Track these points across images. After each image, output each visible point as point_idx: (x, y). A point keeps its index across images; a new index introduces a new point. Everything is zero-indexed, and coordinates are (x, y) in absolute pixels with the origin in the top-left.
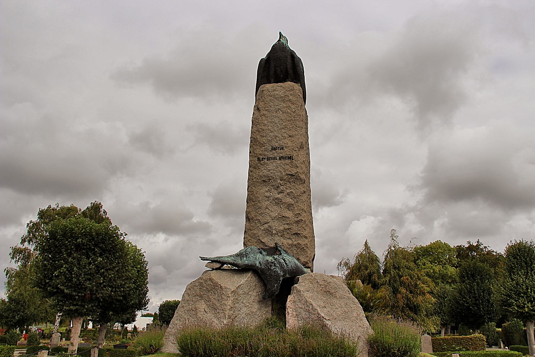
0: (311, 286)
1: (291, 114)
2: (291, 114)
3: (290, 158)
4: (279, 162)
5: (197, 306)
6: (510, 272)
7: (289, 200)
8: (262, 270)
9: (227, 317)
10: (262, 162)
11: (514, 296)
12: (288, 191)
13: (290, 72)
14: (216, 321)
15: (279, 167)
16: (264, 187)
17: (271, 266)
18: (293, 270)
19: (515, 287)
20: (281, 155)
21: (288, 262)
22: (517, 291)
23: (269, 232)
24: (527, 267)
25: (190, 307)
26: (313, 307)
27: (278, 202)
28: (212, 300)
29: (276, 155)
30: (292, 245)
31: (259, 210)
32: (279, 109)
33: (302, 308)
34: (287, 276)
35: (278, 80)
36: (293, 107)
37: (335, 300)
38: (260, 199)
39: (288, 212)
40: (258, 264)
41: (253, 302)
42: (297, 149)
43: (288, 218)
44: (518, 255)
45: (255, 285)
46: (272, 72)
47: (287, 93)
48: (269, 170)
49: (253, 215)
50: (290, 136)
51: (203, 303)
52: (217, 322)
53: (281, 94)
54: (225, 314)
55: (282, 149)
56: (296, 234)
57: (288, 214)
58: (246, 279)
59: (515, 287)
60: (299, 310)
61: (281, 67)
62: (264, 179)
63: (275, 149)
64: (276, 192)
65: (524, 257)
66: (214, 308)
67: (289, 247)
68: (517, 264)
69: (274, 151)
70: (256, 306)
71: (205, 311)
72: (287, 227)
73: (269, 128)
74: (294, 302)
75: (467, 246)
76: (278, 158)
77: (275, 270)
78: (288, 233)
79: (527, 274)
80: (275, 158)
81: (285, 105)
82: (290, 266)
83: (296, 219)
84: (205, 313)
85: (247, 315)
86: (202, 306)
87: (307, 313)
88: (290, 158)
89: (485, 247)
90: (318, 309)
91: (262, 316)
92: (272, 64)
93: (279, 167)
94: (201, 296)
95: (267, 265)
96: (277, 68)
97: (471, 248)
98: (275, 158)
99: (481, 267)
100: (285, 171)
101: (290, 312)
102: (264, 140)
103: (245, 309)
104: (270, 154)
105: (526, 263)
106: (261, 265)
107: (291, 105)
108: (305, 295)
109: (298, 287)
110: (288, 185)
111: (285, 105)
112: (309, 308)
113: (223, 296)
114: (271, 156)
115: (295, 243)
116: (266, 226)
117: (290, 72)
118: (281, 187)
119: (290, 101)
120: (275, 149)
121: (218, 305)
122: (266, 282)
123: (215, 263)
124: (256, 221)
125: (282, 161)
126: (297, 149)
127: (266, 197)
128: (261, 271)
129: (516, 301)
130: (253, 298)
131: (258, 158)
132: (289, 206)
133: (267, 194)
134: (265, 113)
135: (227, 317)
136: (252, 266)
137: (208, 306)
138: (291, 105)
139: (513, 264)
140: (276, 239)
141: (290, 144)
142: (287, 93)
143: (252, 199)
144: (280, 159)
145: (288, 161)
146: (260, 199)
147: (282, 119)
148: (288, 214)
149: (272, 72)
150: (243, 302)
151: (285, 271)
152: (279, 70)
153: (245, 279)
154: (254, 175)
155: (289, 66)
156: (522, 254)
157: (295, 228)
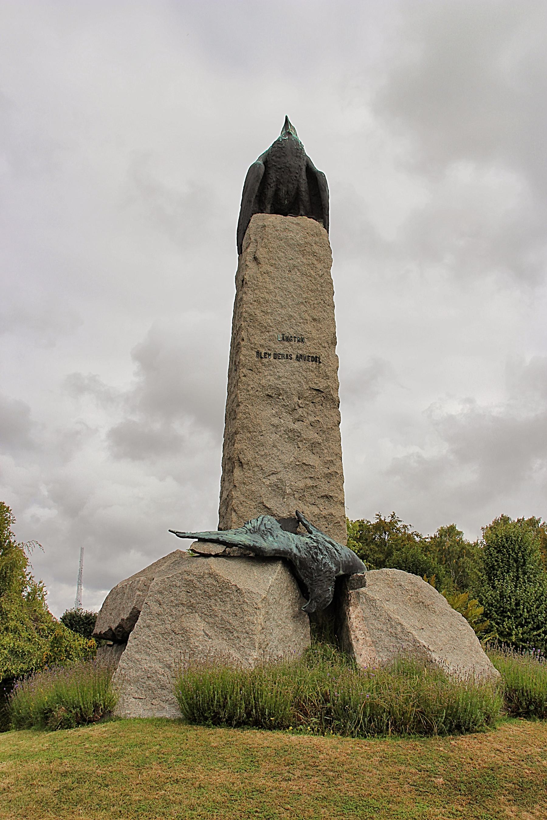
0: (391, 591)
1: (315, 279)
2: (315, 279)
3: (316, 359)
4: (297, 364)
5: (184, 625)
6: (488, 574)
7: (312, 435)
8: (302, 561)
9: (257, 645)
10: (264, 360)
11: (495, 615)
12: (312, 419)
13: (305, 197)
14: (236, 655)
15: (281, 372)
16: (269, 407)
17: (316, 554)
18: (349, 562)
19: (497, 601)
20: (300, 352)
21: (338, 548)
22: (501, 607)
23: (278, 489)
24: (517, 568)
25: (168, 626)
26: (403, 629)
27: (294, 437)
28: (220, 614)
29: (290, 351)
30: (319, 517)
31: (261, 448)
32: (294, 266)
33: (382, 630)
34: (341, 572)
35: (279, 209)
36: (319, 266)
37: (434, 617)
38: (263, 429)
39: (312, 456)
40: (295, 551)
41: (286, 618)
42: (326, 345)
43: (313, 467)
44: (503, 547)
45: (287, 586)
46: (270, 192)
47: (309, 239)
48: (279, 377)
49: (249, 457)
50: (314, 320)
51: (199, 619)
52: (238, 656)
53: (299, 237)
54: (252, 640)
55: (302, 340)
56: (326, 496)
57: (312, 459)
58: (274, 577)
59: (497, 601)
60: (377, 634)
61: (286, 187)
62: (269, 392)
63: (288, 339)
64: (290, 418)
65: (513, 550)
66: (226, 630)
67: (314, 519)
68: (502, 562)
69: (286, 343)
70: (291, 626)
71: (207, 635)
72: (310, 483)
73: (278, 298)
74: (365, 619)
75: (374, 521)
76: (294, 357)
77: (324, 561)
78: (311, 495)
79: (518, 579)
80: (288, 357)
81: (305, 261)
82: (343, 555)
83: (326, 471)
84: (207, 638)
85: (281, 640)
86: (197, 625)
87: (394, 639)
88: (316, 359)
89: (405, 527)
90: (414, 633)
91: (300, 644)
92: (273, 176)
93: (281, 372)
94: (191, 606)
95: (309, 552)
96: (281, 186)
97: (381, 526)
98: (288, 357)
99: (424, 562)
100: (307, 383)
101: (359, 637)
102: (268, 320)
103: (277, 631)
104: (280, 348)
105: (516, 561)
106: (300, 551)
107: (316, 262)
108: (386, 607)
109: (370, 594)
110: (311, 407)
111: (305, 261)
112: (396, 631)
113: (245, 607)
114: (282, 352)
115: (325, 512)
116: (274, 478)
117: (305, 197)
118: (300, 411)
119: (314, 254)
120: (288, 339)
121: (236, 623)
122: (307, 581)
123: (211, 545)
124: (256, 469)
125: (302, 363)
126: (326, 345)
127: (273, 425)
128: (300, 562)
129: (497, 623)
130: (285, 611)
131: (258, 352)
132: (314, 446)
133: (275, 421)
134: (271, 269)
135: (257, 645)
136: (285, 552)
137: (212, 625)
138: (316, 262)
139: (496, 561)
140: (292, 504)
141: (314, 334)
142: (309, 239)
143: (247, 428)
144: (299, 358)
145: (312, 365)
146: (263, 429)
147: (300, 287)
148: (312, 459)
149: (270, 192)
150: (274, 619)
151: (337, 564)
152: (284, 189)
153: (274, 577)
154: (251, 383)
155: (304, 186)
156: (512, 546)
157: (325, 487)
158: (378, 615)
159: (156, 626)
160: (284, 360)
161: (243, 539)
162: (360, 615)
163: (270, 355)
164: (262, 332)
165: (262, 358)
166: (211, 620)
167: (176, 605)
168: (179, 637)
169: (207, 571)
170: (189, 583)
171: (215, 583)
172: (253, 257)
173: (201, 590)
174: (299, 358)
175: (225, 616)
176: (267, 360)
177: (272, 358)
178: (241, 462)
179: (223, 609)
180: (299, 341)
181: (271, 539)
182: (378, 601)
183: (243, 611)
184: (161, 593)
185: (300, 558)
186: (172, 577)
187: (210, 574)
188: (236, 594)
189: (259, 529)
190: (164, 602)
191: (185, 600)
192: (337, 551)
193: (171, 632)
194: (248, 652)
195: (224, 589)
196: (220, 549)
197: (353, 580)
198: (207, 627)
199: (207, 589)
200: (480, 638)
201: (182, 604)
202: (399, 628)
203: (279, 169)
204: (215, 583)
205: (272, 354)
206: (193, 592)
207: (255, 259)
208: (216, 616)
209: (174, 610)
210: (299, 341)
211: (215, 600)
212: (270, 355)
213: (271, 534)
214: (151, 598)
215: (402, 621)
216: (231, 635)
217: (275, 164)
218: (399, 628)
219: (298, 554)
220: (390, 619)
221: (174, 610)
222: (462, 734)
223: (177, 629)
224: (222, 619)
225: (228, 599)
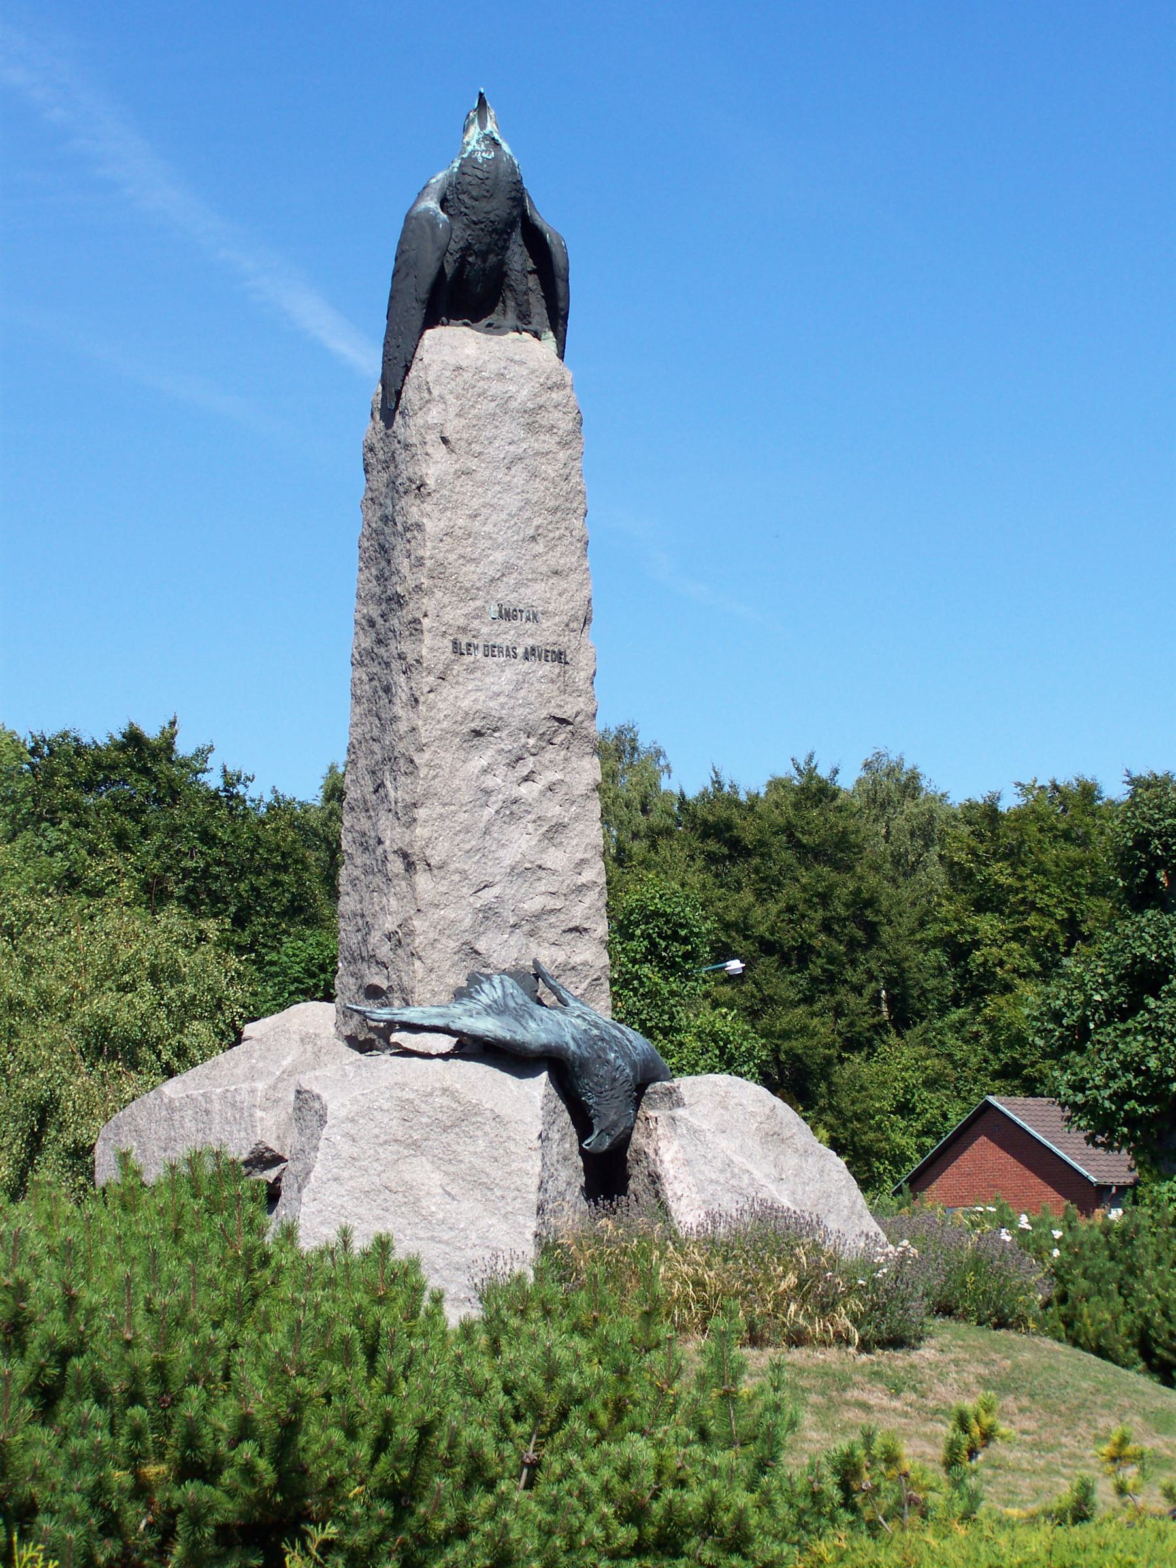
3: (559, 657)
5: (407, 1177)
25: (376, 1180)
33: (717, 1182)
40: (573, 1046)
51: (429, 1167)
56: (576, 929)
60: (710, 1188)
71: (449, 1194)
95: (591, 1047)
102: (470, 574)
113: (511, 1146)
137: (454, 1177)
144: (531, 653)
158: (709, 1156)
159: (351, 1178)
160: (502, 659)
161: (491, 1027)
162: (680, 1156)
163: (476, 648)
164: (461, 600)
165: (462, 654)
166: (452, 1169)
167: (386, 1142)
168: (400, 1197)
169: (438, 1085)
170: (403, 1104)
171: (455, 1105)
172: (438, 435)
173: (429, 1117)
174: (531, 653)
175: (477, 1162)
176: (472, 658)
177: (480, 655)
178: (429, 865)
179: (471, 1149)
180: (528, 619)
181: (533, 1025)
182: (708, 1134)
183: (507, 1153)
184: (353, 1121)
185: (582, 1058)
186: (372, 1092)
187: (445, 1090)
188: (493, 1124)
189: (506, 1005)
190: (361, 1138)
191: (400, 1134)
192: (631, 1042)
193: (382, 1189)
194: (522, 1222)
195: (464, 1117)
196: (446, 1043)
197: (655, 1093)
198: (446, 1180)
199: (440, 1116)
200: (194, 1065)
201: (396, 1141)
202: (746, 1178)
203: (475, 223)
204: (455, 1105)
205: (481, 645)
206: (415, 1121)
207: (445, 441)
208: (461, 1161)
209: (380, 1150)
210: (528, 619)
211: (457, 1134)
212: (476, 648)
213: (531, 1016)
214: (335, 1129)
215: (750, 1167)
216: (489, 1193)
217: (466, 211)
218: (746, 1178)
219: (578, 1052)
220: (730, 1164)
221: (380, 1150)
222: (914, 1348)
223: (394, 1184)
224: (472, 1167)
225: (479, 1133)
